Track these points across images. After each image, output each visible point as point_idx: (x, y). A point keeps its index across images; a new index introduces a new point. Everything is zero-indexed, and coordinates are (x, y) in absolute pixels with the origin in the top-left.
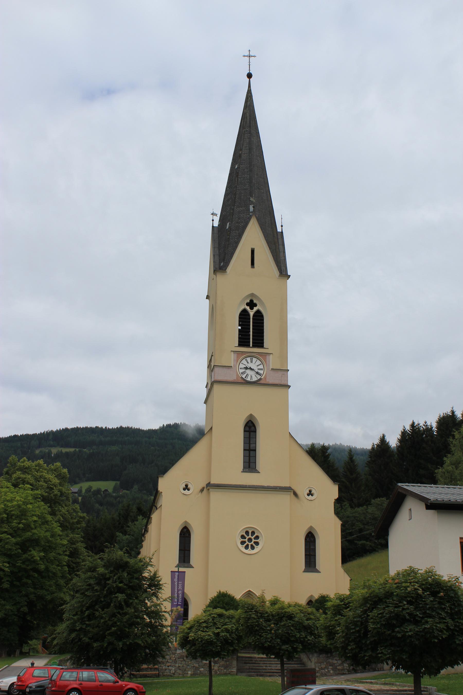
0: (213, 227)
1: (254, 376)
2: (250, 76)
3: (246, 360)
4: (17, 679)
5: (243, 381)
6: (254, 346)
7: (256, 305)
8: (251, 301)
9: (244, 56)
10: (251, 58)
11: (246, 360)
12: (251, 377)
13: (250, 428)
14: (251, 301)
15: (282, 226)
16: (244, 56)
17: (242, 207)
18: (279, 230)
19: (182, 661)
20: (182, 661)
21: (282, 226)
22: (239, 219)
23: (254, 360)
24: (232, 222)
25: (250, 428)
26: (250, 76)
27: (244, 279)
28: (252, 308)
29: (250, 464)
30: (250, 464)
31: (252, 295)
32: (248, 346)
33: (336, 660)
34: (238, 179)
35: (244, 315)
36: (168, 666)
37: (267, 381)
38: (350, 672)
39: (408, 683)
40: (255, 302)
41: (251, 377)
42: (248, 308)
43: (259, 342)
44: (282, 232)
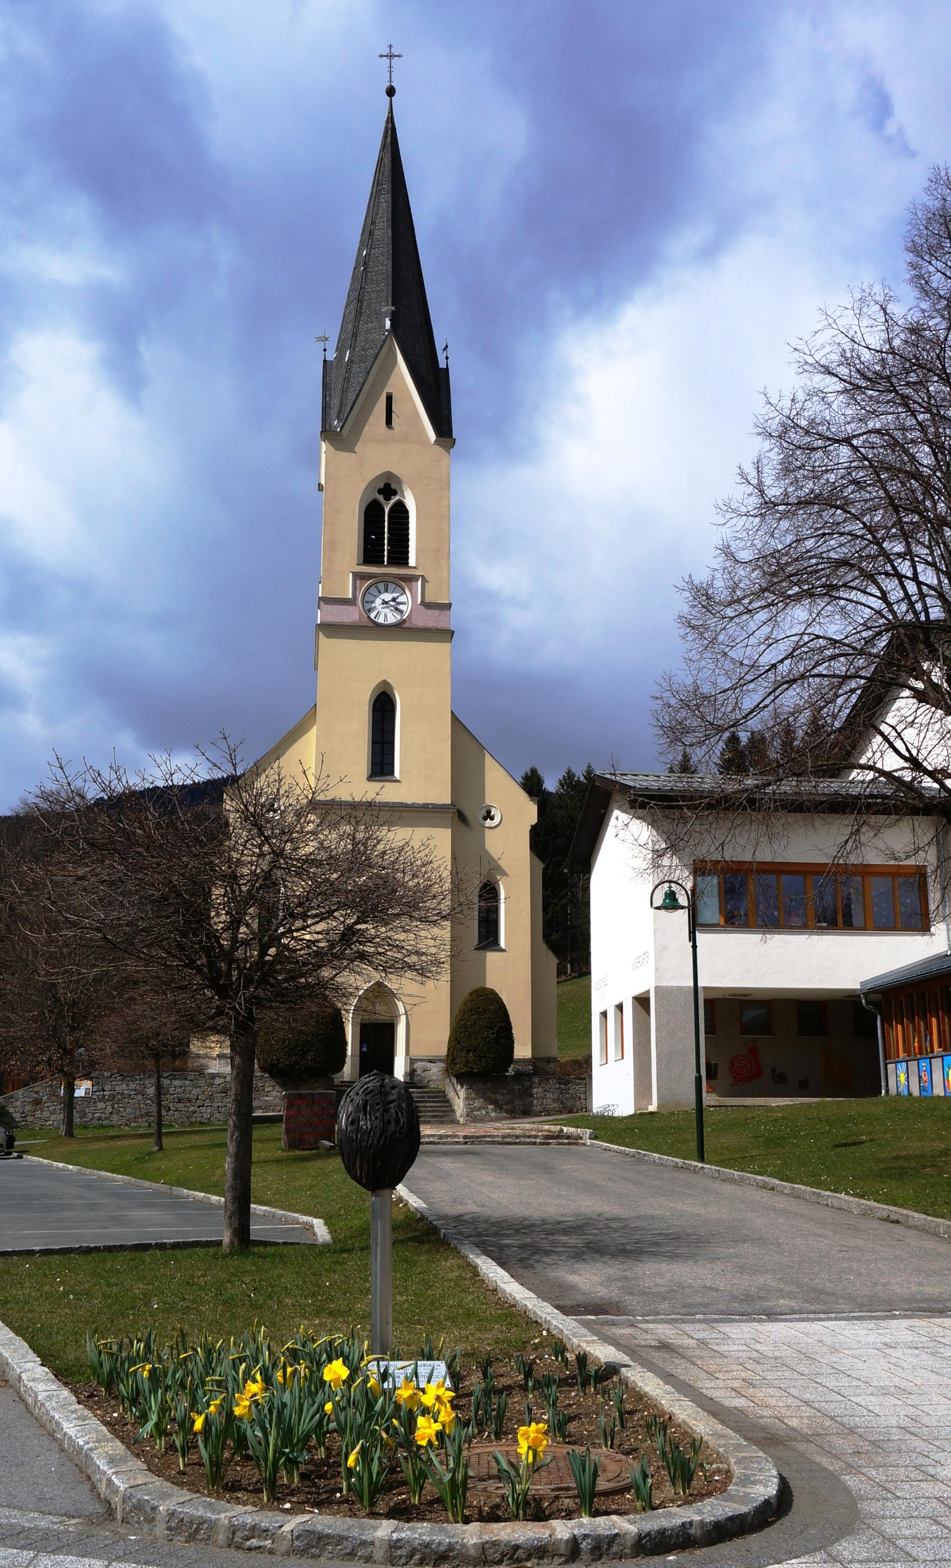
0: (325, 361)
1: (390, 615)
2: (391, 92)
3: (377, 588)
4: (938, 1096)
5: (370, 624)
6: (391, 563)
7: (395, 493)
8: (387, 486)
9: (381, 56)
10: (395, 60)
11: (377, 588)
12: (386, 616)
13: (383, 707)
14: (387, 486)
15: (447, 358)
16: (381, 56)
17: (372, 323)
18: (442, 365)
19: (223, 1097)
20: (223, 1097)
21: (447, 358)
22: (367, 343)
23: (391, 586)
24: (354, 349)
25: (383, 707)
26: (391, 92)
27: (377, 454)
28: (388, 499)
29: (381, 765)
30: (381, 765)
31: (389, 474)
32: (378, 561)
33: (502, 1094)
34: (366, 275)
35: (372, 514)
36: (199, 1107)
37: (414, 622)
38: (510, 1118)
39: (265, 1205)
40: (393, 486)
41: (386, 616)
42: (381, 498)
43: (400, 556)
44: (447, 369)
